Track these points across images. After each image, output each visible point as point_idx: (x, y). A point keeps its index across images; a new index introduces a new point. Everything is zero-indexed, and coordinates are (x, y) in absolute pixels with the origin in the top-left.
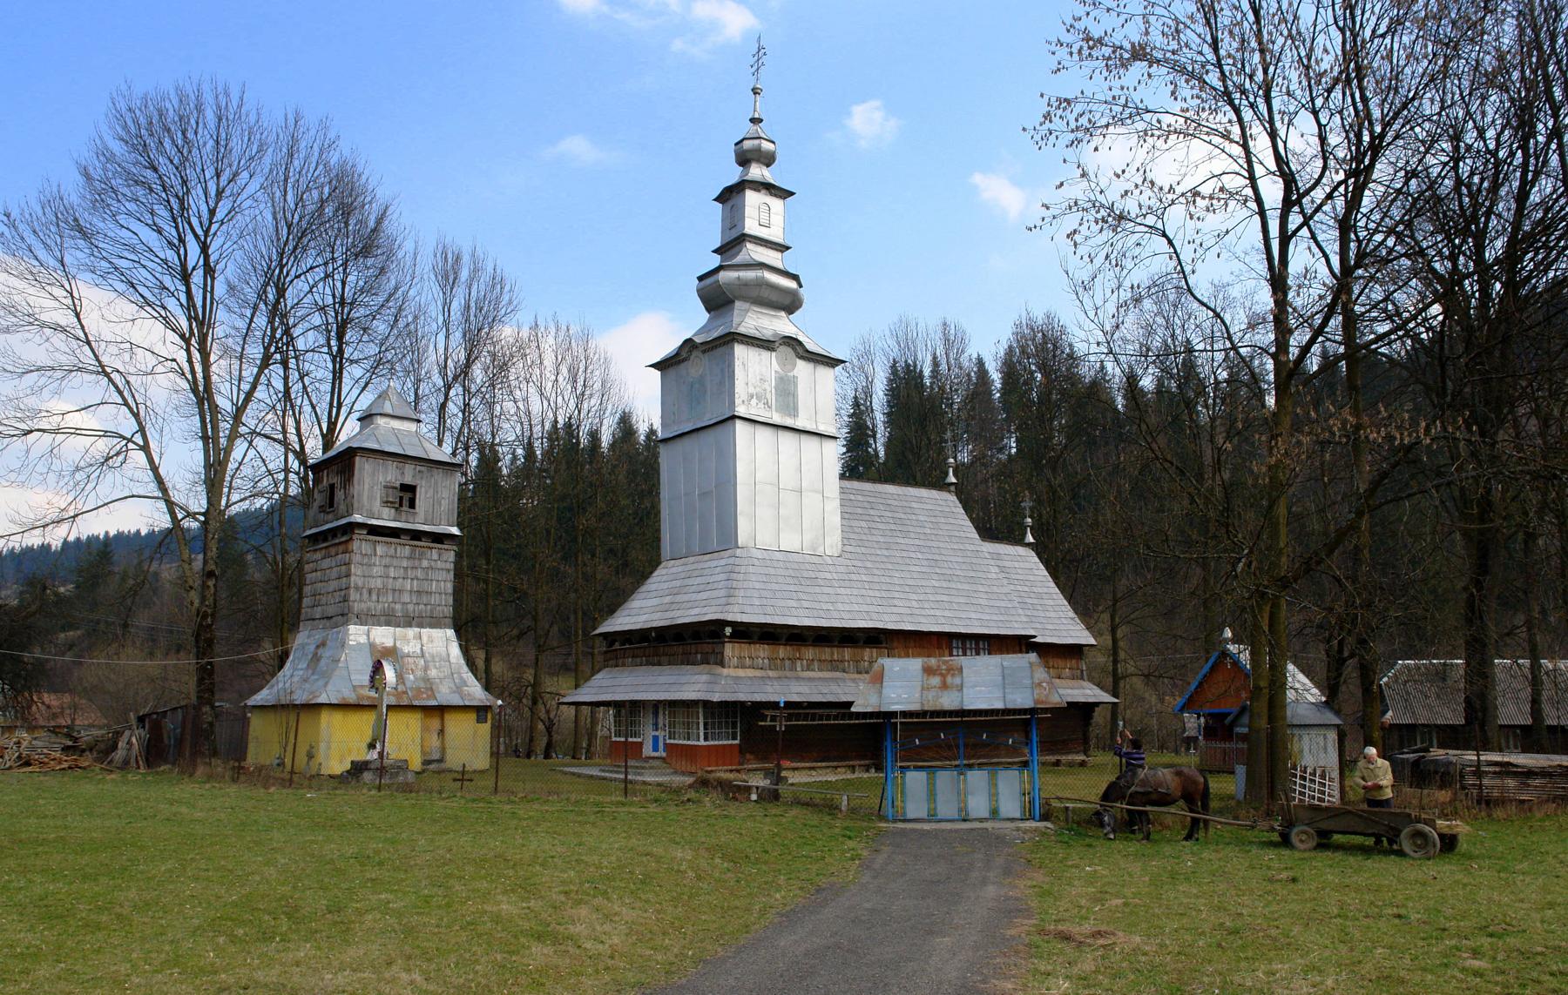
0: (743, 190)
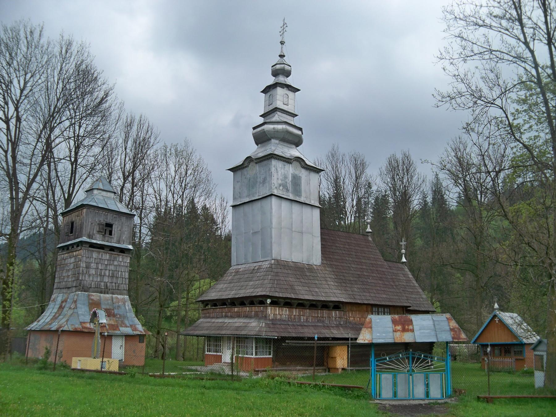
0: (276, 87)
